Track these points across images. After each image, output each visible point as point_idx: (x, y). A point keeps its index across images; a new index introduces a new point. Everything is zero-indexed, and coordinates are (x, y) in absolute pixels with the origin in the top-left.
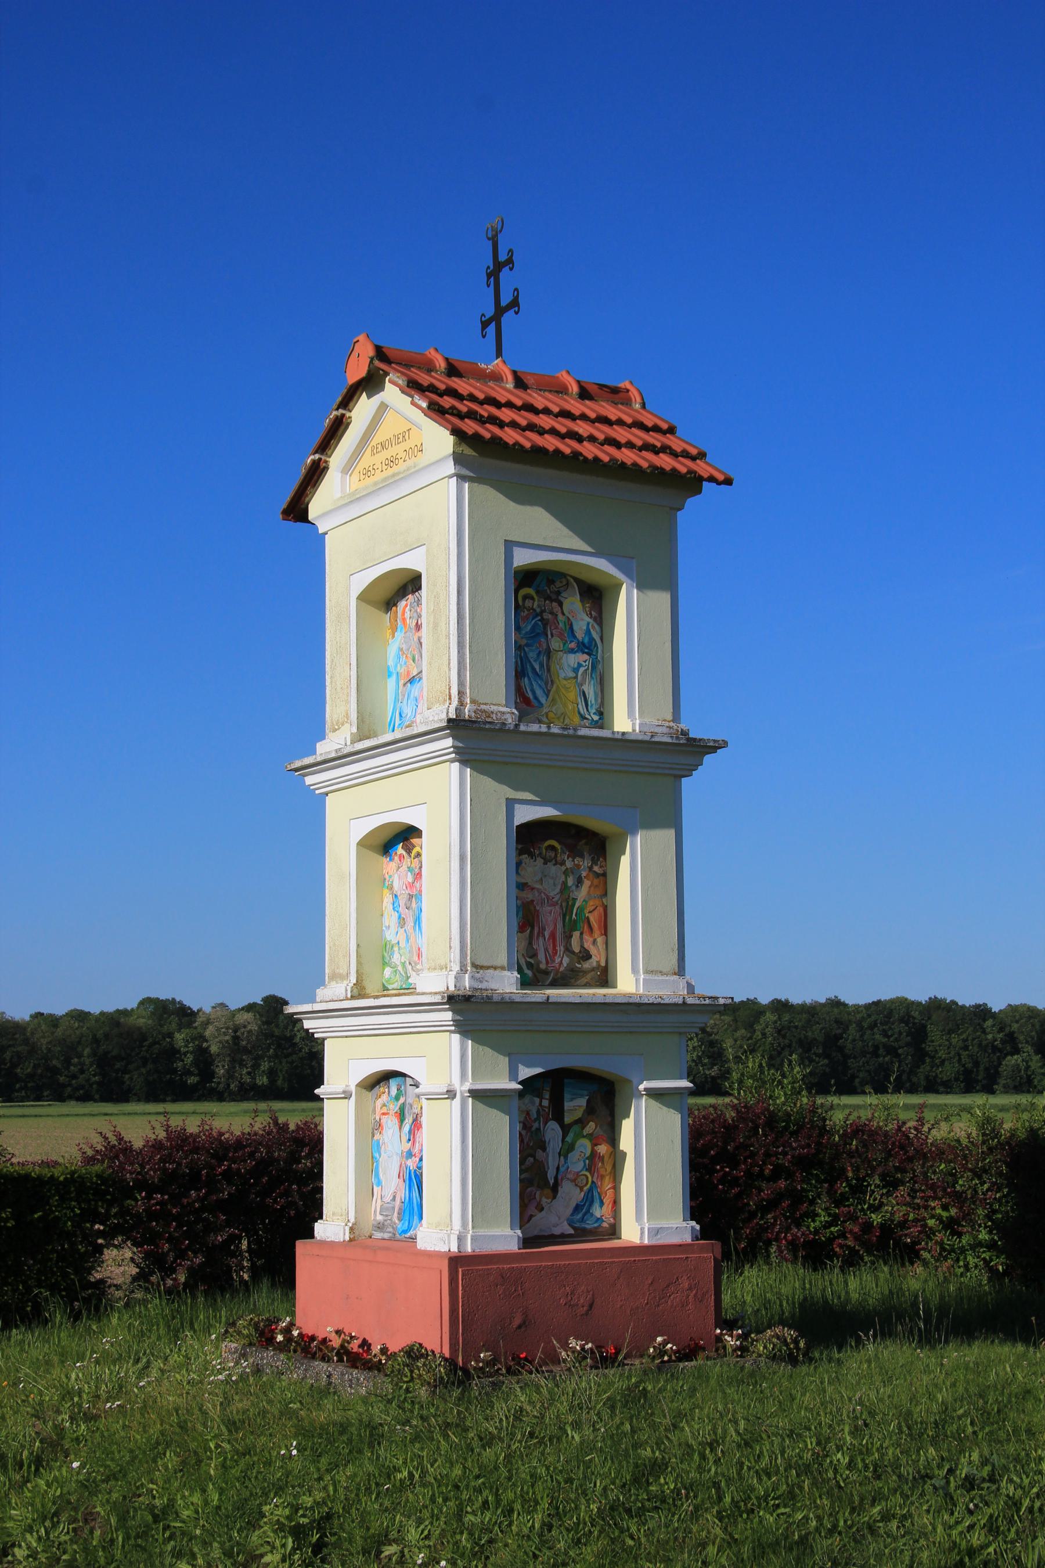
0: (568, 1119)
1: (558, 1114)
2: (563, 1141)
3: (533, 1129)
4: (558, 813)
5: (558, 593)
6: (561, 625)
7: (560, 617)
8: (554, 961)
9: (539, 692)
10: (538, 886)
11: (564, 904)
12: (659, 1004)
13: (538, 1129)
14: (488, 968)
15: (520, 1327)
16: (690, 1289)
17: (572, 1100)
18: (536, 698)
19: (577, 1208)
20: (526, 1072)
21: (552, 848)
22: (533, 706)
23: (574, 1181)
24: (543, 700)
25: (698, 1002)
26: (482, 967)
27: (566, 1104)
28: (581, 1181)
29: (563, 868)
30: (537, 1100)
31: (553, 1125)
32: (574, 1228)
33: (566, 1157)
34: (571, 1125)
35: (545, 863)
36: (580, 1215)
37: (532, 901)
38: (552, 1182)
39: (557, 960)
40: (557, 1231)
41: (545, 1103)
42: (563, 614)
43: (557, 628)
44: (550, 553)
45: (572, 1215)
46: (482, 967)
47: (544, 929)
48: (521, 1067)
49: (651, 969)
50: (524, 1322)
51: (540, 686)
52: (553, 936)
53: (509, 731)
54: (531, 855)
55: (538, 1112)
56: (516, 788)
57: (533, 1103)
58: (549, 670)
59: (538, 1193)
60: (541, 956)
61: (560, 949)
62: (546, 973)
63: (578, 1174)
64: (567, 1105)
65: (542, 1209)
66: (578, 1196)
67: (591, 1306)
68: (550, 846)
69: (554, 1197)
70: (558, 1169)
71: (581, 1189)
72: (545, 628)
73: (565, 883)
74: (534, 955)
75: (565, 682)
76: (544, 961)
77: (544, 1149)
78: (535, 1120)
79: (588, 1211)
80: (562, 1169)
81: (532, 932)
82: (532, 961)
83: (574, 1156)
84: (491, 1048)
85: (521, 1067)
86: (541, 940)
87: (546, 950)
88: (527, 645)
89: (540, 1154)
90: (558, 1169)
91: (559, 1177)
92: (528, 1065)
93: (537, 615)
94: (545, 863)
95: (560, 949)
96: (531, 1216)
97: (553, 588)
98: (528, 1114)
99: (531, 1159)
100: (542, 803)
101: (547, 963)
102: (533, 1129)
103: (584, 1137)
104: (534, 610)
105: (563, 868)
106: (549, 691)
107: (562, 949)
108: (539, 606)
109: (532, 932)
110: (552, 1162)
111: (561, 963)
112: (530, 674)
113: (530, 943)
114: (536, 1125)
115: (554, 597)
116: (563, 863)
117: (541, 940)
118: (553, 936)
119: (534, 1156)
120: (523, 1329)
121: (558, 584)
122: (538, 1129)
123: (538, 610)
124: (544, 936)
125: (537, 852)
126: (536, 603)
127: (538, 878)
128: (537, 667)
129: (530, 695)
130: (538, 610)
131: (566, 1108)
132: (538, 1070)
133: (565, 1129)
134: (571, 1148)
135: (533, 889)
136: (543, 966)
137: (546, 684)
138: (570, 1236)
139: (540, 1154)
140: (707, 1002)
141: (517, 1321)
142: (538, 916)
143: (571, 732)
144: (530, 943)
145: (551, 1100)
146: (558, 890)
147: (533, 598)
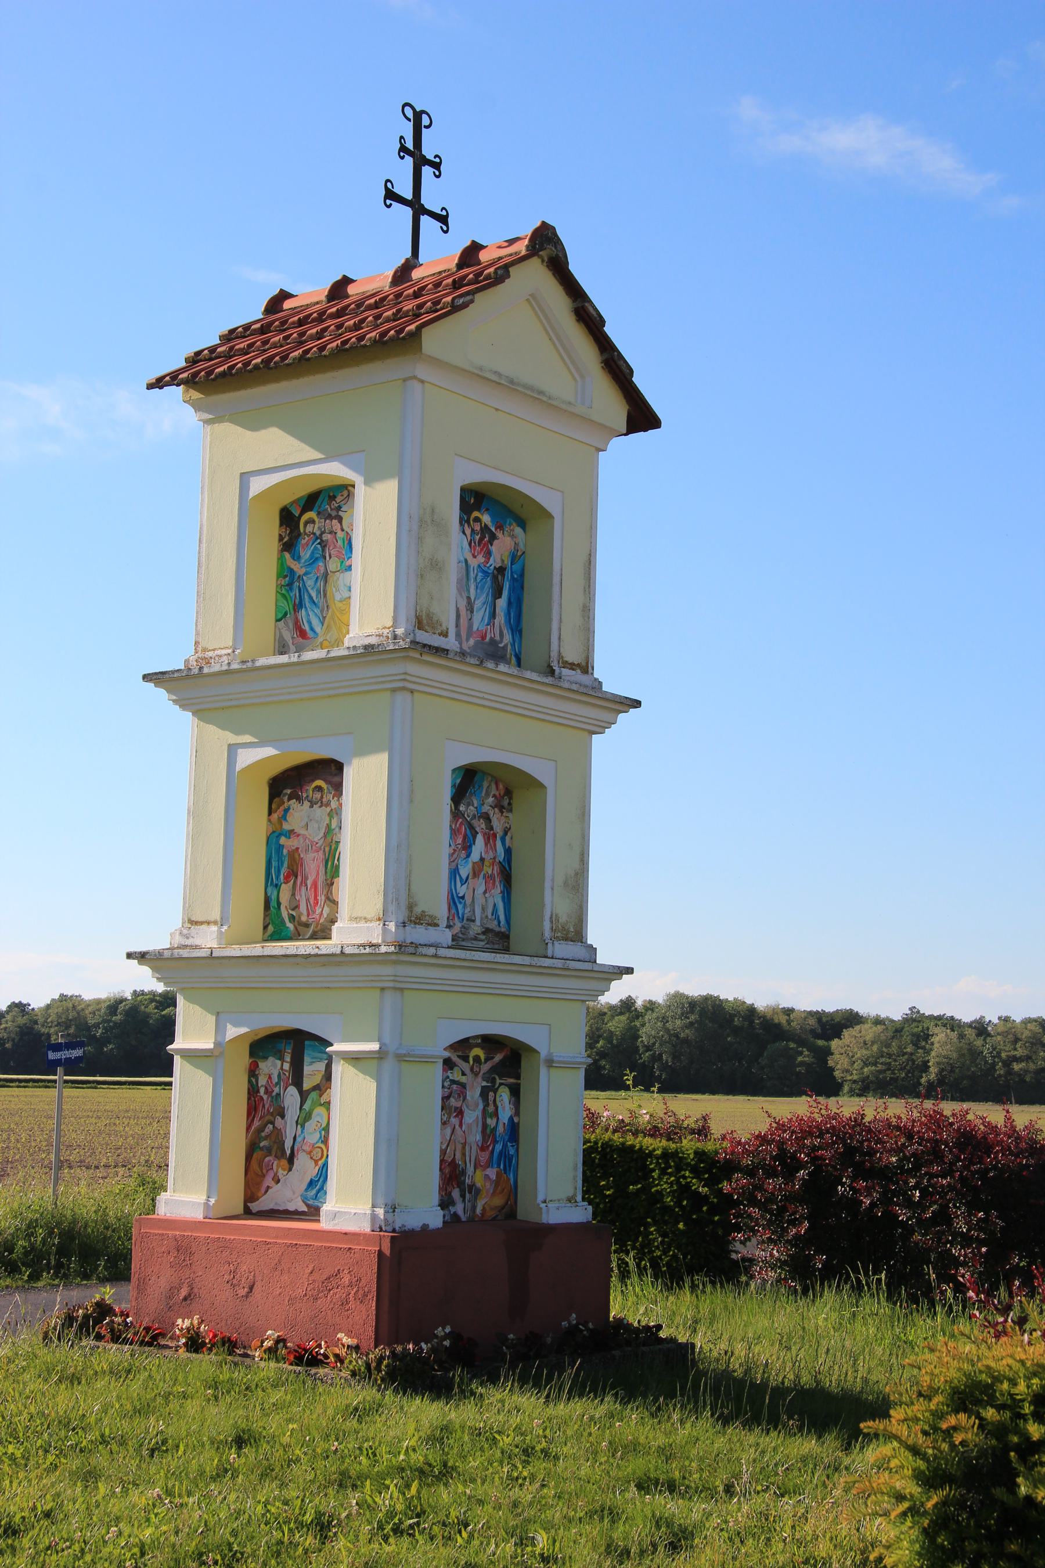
0: (307, 1085)
1: (297, 1079)
2: (301, 1109)
3: (274, 1094)
4: (269, 751)
5: (339, 508)
6: (340, 542)
7: (340, 535)
8: (314, 912)
9: (315, 622)
10: (303, 832)
11: (327, 849)
12: (317, 955)
13: (278, 1095)
14: (202, 923)
15: (185, 1299)
16: (351, 1285)
17: (312, 1063)
18: (312, 629)
19: (311, 1184)
20: (232, 1032)
21: (319, 789)
22: (308, 638)
23: (310, 1153)
24: (318, 629)
25: (357, 951)
26: (197, 923)
27: (305, 1068)
28: (317, 1154)
29: (328, 809)
30: (279, 1063)
31: (292, 1090)
32: (308, 1205)
33: (303, 1126)
34: (309, 1092)
35: (311, 807)
36: (314, 1192)
37: (297, 849)
38: (288, 1152)
39: (318, 911)
40: (291, 1208)
41: (286, 1066)
42: (343, 530)
43: (335, 547)
44: (283, 473)
45: (306, 1190)
46: (197, 923)
47: (306, 878)
48: (229, 1026)
49: (354, 915)
50: (190, 1295)
51: (316, 615)
52: (315, 885)
53: (195, 676)
54: (299, 799)
55: (279, 1075)
56: (238, 732)
57: (275, 1066)
58: (325, 595)
59: (275, 1163)
60: (303, 908)
61: (322, 898)
62: (307, 925)
63: (313, 1146)
64: (307, 1069)
65: (278, 1181)
66: (312, 1171)
67: (251, 1288)
68: (317, 787)
69: (290, 1170)
70: (295, 1138)
71: (316, 1162)
72: (323, 551)
73: (328, 826)
74: (296, 907)
75: (341, 605)
76: (305, 912)
77: (283, 1117)
78: (277, 1084)
79: (322, 1188)
80: (299, 1139)
81: (295, 882)
82: (294, 913)
83: (310, 1125)
84: (201, 1006)
85: (229, 1026)
86: (303, 889)
87: (308, 900)
88: (306, 574)
89: (279, 1122)
90: (295, 1138)
91: (296, 1148)
92: (236, 1025)
93: (317, 538)
94: (311, 807)
95: (322, 898)
96: (268, 1187)
97: (334, 504)
98: (270, 1077)
99: (271, 1126)
100: (261, 744)
101: (308, 915)
102: (274, 1094)
103: (321, 1105)
104: (314, 534)
105: (328, 809)
106: (324, 618)
107: (323, 898)
108: (319, 528)
109: (295, 882)
110: (289, 1128)
111: (321, 914)
112: (308, 604)
113: (293, 895)
114: (276, 1090)
115: (334, 513)
116: (328, 804)
117: (303, 889)
118: (315, 885)
119: (273, 1123)
120: (188, 1302)
121: (338, 499)
122: (278, 1095)
123: (318, 533)
124: (306, 885)
125: (305, 795)
126: (316, 526)
127: (303, 823)
128: (314, 594)
129: (307, 627)
130: (318, 533)
131: (305, 1073)
132: (243, 1030)
133: (304, 1095)
134: (308, 1117)
135: (298, 835)
136: (304, 918)
137: (322, 611)
138: (303, 1213)
139: (279, 1122)
140: (368, 950)
141: (184, 1292)
142: (302, 865)
143: (249, 664)
144: (293, 895)
145: (292, 1064)
146: (322, 834)
147: (313, 522)
